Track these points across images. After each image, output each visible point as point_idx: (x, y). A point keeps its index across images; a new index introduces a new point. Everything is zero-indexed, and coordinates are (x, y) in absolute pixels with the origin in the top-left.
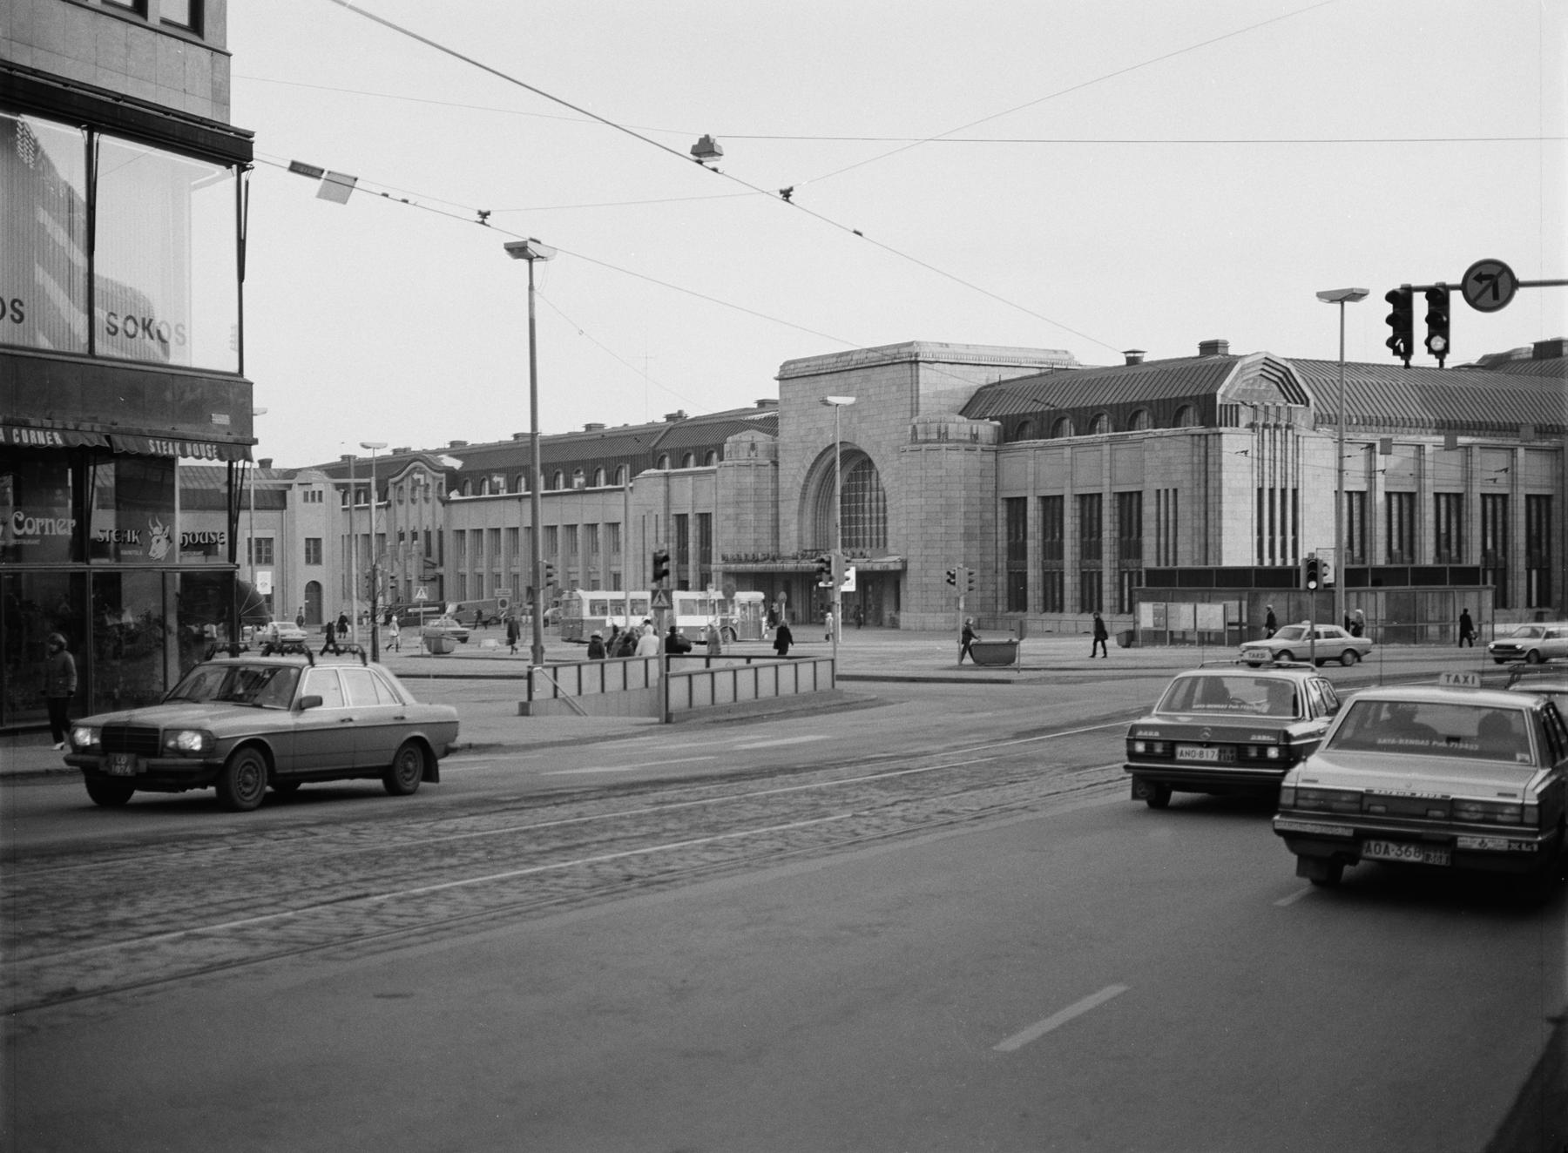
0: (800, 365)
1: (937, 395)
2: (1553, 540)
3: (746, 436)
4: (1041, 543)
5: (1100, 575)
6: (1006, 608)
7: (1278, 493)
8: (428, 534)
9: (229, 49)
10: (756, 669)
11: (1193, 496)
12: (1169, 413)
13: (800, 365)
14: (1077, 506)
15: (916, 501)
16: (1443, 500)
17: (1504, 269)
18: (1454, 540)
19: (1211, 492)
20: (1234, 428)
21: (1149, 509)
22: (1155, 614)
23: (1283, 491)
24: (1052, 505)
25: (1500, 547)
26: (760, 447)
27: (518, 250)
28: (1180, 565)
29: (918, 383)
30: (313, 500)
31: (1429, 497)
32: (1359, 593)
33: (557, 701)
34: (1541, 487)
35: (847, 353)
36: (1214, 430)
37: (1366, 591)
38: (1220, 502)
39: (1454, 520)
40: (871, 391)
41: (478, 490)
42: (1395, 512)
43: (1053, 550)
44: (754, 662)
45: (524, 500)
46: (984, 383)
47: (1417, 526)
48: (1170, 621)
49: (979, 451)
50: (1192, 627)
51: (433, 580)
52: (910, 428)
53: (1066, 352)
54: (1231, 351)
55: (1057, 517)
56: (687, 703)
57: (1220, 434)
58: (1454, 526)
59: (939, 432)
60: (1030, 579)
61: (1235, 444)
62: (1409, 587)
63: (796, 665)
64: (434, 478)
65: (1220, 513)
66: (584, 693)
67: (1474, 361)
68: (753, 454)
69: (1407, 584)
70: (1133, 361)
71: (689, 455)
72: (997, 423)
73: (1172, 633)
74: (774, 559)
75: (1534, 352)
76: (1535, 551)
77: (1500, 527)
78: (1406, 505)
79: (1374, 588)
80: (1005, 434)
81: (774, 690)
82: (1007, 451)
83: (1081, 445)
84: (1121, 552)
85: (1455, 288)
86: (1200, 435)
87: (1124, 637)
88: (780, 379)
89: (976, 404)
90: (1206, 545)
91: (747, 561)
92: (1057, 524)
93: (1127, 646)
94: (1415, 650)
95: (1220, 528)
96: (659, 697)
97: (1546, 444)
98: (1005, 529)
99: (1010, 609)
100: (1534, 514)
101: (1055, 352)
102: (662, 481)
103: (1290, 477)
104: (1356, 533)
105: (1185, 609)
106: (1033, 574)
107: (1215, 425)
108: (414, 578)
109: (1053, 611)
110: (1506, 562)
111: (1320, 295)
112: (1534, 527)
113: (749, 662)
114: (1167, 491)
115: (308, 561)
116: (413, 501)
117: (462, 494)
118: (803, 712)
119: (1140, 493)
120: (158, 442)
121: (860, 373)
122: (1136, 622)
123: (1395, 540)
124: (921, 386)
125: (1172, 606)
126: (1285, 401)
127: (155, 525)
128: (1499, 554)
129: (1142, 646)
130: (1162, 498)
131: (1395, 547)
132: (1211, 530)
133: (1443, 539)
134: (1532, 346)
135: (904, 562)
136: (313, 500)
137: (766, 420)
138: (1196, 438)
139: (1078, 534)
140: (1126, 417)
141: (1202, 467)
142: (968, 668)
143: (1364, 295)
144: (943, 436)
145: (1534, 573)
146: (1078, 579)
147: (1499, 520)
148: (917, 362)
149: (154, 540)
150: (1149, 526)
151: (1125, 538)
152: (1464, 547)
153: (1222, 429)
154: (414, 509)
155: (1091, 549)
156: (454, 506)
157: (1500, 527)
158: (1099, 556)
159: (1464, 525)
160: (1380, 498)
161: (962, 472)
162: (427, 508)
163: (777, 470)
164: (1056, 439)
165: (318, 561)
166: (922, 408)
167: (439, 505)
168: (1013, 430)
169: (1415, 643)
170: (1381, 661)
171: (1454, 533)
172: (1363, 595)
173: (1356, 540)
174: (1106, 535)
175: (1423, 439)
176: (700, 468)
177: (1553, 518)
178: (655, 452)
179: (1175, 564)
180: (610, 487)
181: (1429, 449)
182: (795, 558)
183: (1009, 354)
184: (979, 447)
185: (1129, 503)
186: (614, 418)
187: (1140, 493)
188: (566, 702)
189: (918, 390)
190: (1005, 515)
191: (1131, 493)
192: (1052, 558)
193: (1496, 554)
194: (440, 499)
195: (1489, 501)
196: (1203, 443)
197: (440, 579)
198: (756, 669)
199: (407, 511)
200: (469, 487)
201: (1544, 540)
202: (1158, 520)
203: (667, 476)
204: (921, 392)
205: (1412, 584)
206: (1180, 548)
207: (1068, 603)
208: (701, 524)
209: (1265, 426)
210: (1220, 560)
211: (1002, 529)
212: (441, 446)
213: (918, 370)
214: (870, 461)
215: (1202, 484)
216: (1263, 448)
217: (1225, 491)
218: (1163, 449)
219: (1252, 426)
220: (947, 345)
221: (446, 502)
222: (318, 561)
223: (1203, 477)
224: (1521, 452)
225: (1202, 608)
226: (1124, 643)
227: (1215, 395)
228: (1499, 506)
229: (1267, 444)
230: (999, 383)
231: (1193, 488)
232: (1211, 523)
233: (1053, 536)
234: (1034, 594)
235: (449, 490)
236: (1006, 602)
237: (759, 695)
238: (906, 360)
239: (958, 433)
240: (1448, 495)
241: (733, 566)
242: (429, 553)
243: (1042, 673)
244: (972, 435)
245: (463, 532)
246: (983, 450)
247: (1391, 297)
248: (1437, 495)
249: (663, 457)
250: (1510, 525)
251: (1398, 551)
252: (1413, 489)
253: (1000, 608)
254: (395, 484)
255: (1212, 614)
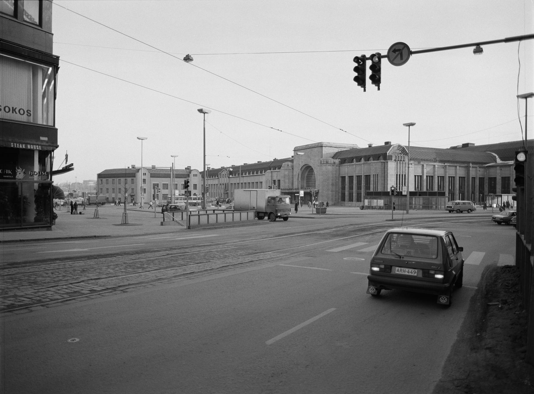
0: (298, 148)
1: (327, 154)
2: (465, 187)
3: (286, 163)
4: (348, 186)
5: (361, 193)
6: (341, 201)
7: (401, 175)
8: (226, 184)
9: (53, 32)
10: (217, 215)
11: (382, 176)
12: (377, 157)
13: (298, 148)
14: (356, 178)
15: (321, 177)
16: (440, 178)
17: (405, 46)
18: (442, 187)
19: (385, 175)
20: (391, 161)
21: (372, 179)
22: (368, 202)
23: (402, 175)
24: (351, 178)
25: (453, 188)
26: (290, 165)
27: (201, 111)
28: (378, 191)
29: (322, 151)
30: (195, 176)
31: (436, 177)
32: (415, 198)
33: (174, 221)
34: (462, 175)
35: (308, 145)
36: (386, 161)
37: (417, 197)
38: (388, 177)
39: (442, 182)
40: (313, 153)
41: (235, 175)
42: (428, 180)
43: (351, 188)
44: (225, 212)
45: (244, 177)
46: (337, 151)
47: (433, 183)
48: (372, 204)
49: (335, 166)
50: (377, 205)
51: (226, 194)
52: (320, 161)
53: (356, 145)
54: (392, 144)
55: (352, 181)
56: (207, 222)
57: (388, 162)
58: (442, 184)
59: (326, 162)
60: (346, 194)
61: (392, 166)
62: (428, 196)
63: (240, 213)
64: (227, 173)
65: (388, 180)
66: (183, 219)
67: (449, 148)
68: (288, 167)
69: (427, 196)
70: (370, 146)
71: (276, 167)
72: (340, 160)
73: (372, 207)
74: (291, 190)
75: (462, 146)
76: (461, 189)
77: (453, 184)
78: (431, 179)
79: (419, 197)
80: (341, 162)
81: (224, 220)
82: (342, 166)
83: (357, 165)
84: (366, 188)
85: (384, 57)
86: (383, 162)
87: (361, 207)
88: (294, 151)
89: (335, 156)
90: (384, 187)
91: (286, 190)
92: (352, 182)
93: (362, 209)
94: (428, 211)
95: (387, 183)
96: (187, 220)
97: (464, 165)
98: (341, 183)
99: (342, 201)
100: (461, 181)
101: (354, 145)
102: (271, 173)
103: (404, 172)
104: (419, 185)
105: (375, 201)
106: (347, 193)
107: (386, 160)
108: (222, 193)
109: (351, 201)
110: (454, 192)
111: (404, 125)
112: (461, 184)
113: (224, 212)
114: (376, 175)
115: (194, 189)
116: (223, 177)
117: (232, 176)
118: (238, 226)
119: (370, 175)
120: (15, 144)
121: (310, 149)
122: (364, 204)
123: (428, 187)
124: (323, 152)
125: (372, 200)
126: (403, 155)
127: (18, 169)
128: (453, 190)
129: (365, 209)
130: (375, 177)
131: (428, 188)
132: (385, 184)
133: (439, 186)
134: (462, 145)
135: (318, 190)
136: (195, 176)
137: (291, 160)
138: (382, 163)
139: (356, 185)
140: (367, 158)
141: (384, 169)
142: (315, 214)
143: (414, 124)
144: (327, 163)
145: (461, 194)
146: (356, 194)
147: (453, 182)
148: (322, 147)
149: (18, 173)
150: (372, 182)
151: (367, 185)
152: (444, 188)
153: (388, 161)
154: (223, 179)
155: (359, 188)
156: (231, 178)
157: (453, 184)
158: (361, 189)
159: (444, 183)
160: (425, 177)
161: (331, 170)
162: (225, 179)
163: (293, 170)
164: (352, 163)
165: (196, 189)
166: (323, 157)
167: (228, 178)
168: (343, 161)
169: (429, 210)
170: (403, 214)
171: (442, 185)
172: (416, 198)
173: (419, 186)
174: (362, 184)
175: (435, 164)
176: (278, 170)
177: (465, 182)
178: (270, 167)
179: (377, 190)
180: (260, 174)
181: (436, 166)
182: (296, 189)
183: (338, 145)
184: (335, 165)
185: (368, 177)
186: (263, 160)
187: (370, 175)
188: (176, 221)
189: (322, 153)
190: (341, 180)
191: (368, 175)
192: (359, 190)
193: (452, 190)
194: (228, 177)
195: (450, 178)
196: (384, 164)
197: (228, 193)
198: (217, 215)
199: (222, 179)
200: (234, 175)
201: (463, 187)
202: (374, 181)
203: (272, 172)
204: (323, 153)
205: (429, 196)
206: (378, 188)
207: (346, 199)
208: (278, 182)
209: (398, 160)
210: (387, 190)
211: (340, 183)
212: (230, 166)
213: (322, 148)
214: (312, 169)
215: (384, 173)
216: (398, 165)
217: (389, 175)
218: (375, 165)
219: (395, 160)
220: (329, 143)
221: (229, 177)
222: (196, 189)
223: (384, 172)
224: (458, 167)
225: (379, 200)
226: (361, 209)
227: (387, 153)
228: (453, 179)
229: (399, 164)
230: (341, 151)
231: (381, 174)
232: (385, 182)
233: (351, 185)
234: (347, 198)
235: (230, 175)
236: (341, 199)
237: (241, 220)
238: (320, 146)
239: (331, 162)
240: (441, 176)
241: (283, 191)
242: (226, 188)
243: (332, 216)
244: (334, 162)
245: (232, 184)
246: (336, 166)
247: (356, 59)
248: (438, 177)
249: (271, 168)
250: (455, 184)
251: (429, 189)
252: (433, 175)
253: (339, 201)
254: (220, 174)
255: (381, 202)
